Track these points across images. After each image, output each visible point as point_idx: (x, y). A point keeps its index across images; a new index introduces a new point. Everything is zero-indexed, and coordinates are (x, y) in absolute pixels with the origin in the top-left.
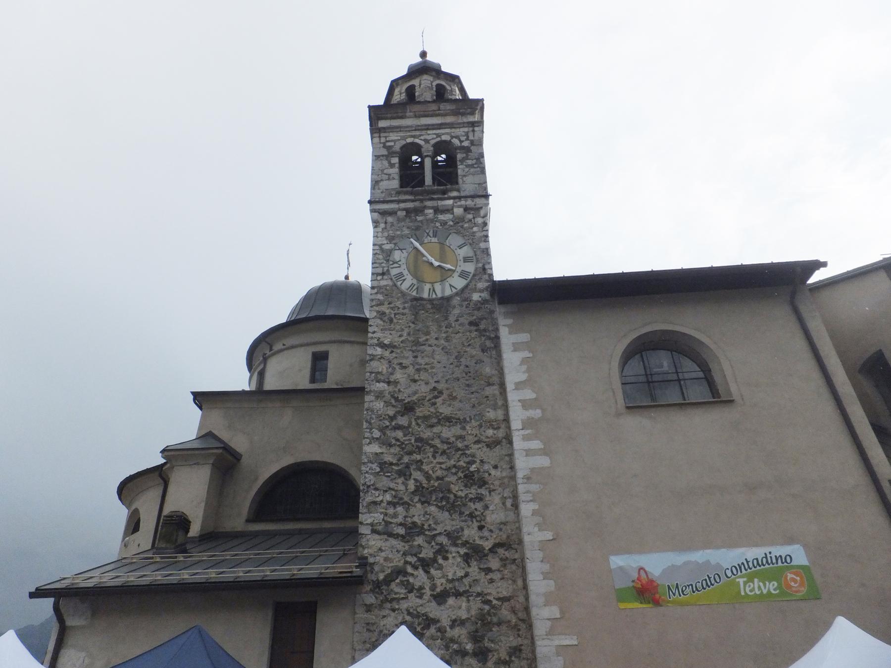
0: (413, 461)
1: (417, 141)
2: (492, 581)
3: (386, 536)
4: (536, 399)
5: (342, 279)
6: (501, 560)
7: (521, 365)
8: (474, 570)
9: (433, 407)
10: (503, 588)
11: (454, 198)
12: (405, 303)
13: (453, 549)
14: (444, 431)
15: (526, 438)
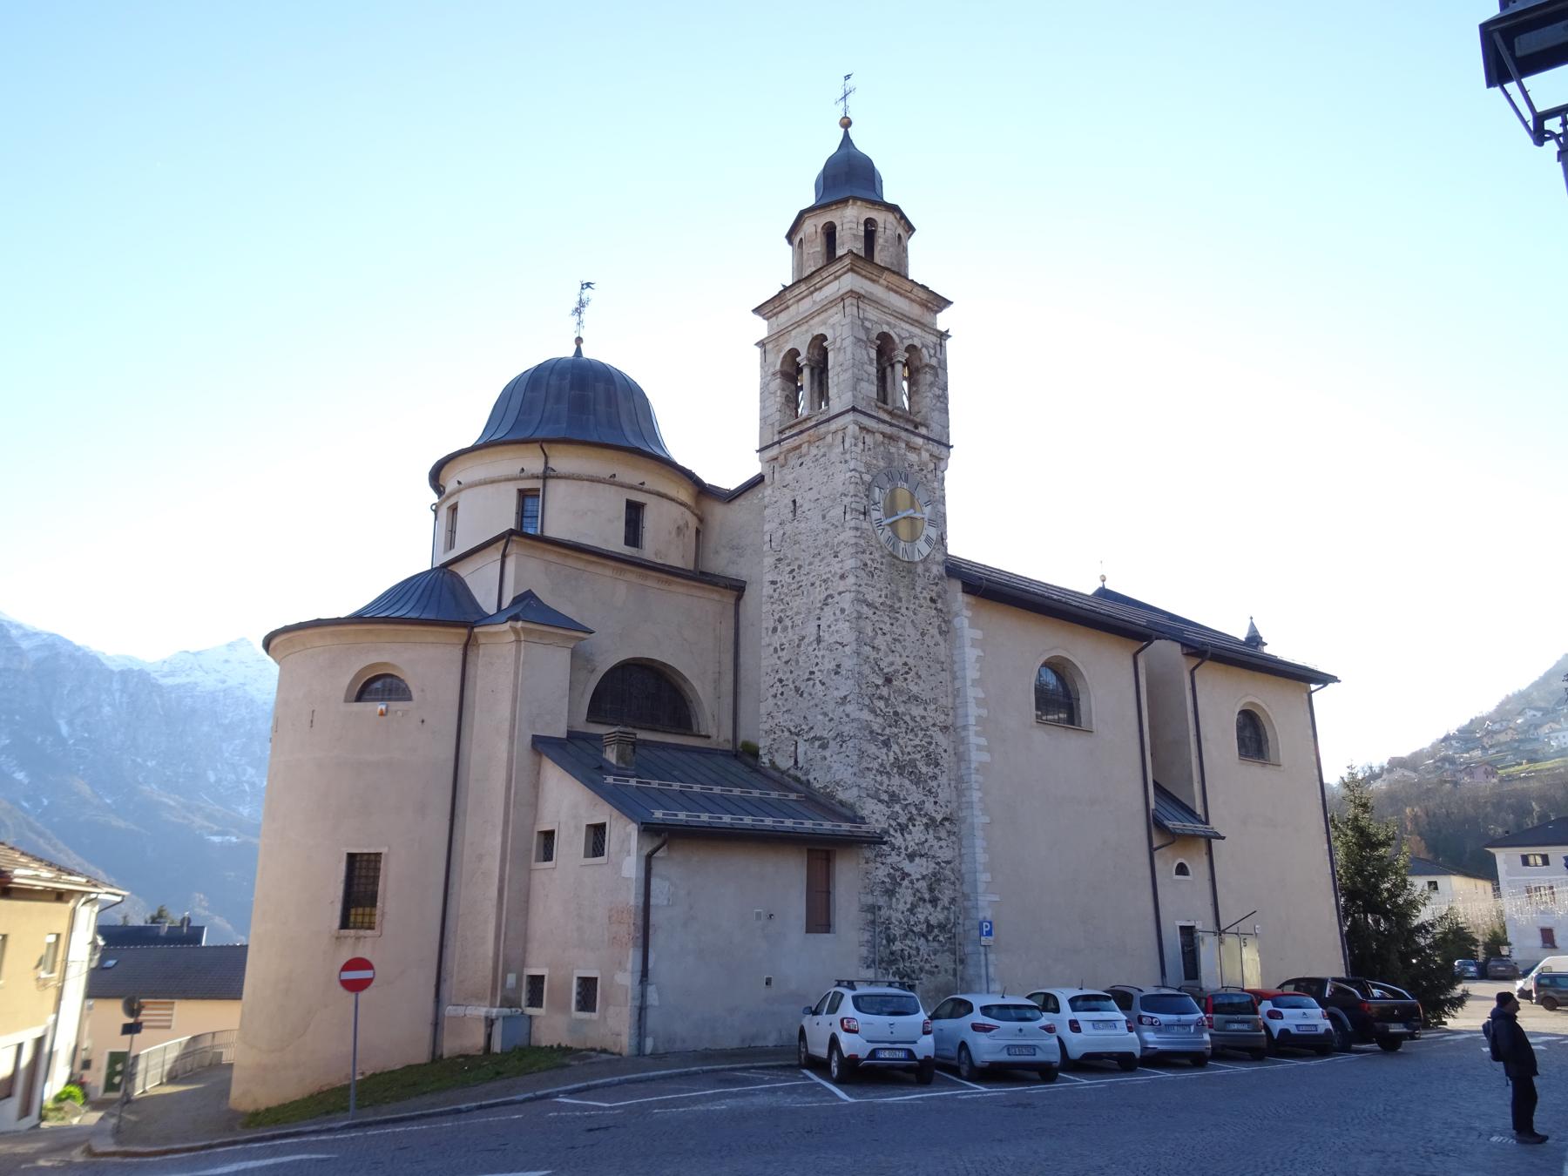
2: (941, 847)
3: (876, 801)
4: (984, 699)
5: (568, 352)
6: (948, 832)
8: (931, 836)
10: (945, 854)
11: (923, 437)
12: (883, 557)
13: (918, 818)
15: (978, 734)
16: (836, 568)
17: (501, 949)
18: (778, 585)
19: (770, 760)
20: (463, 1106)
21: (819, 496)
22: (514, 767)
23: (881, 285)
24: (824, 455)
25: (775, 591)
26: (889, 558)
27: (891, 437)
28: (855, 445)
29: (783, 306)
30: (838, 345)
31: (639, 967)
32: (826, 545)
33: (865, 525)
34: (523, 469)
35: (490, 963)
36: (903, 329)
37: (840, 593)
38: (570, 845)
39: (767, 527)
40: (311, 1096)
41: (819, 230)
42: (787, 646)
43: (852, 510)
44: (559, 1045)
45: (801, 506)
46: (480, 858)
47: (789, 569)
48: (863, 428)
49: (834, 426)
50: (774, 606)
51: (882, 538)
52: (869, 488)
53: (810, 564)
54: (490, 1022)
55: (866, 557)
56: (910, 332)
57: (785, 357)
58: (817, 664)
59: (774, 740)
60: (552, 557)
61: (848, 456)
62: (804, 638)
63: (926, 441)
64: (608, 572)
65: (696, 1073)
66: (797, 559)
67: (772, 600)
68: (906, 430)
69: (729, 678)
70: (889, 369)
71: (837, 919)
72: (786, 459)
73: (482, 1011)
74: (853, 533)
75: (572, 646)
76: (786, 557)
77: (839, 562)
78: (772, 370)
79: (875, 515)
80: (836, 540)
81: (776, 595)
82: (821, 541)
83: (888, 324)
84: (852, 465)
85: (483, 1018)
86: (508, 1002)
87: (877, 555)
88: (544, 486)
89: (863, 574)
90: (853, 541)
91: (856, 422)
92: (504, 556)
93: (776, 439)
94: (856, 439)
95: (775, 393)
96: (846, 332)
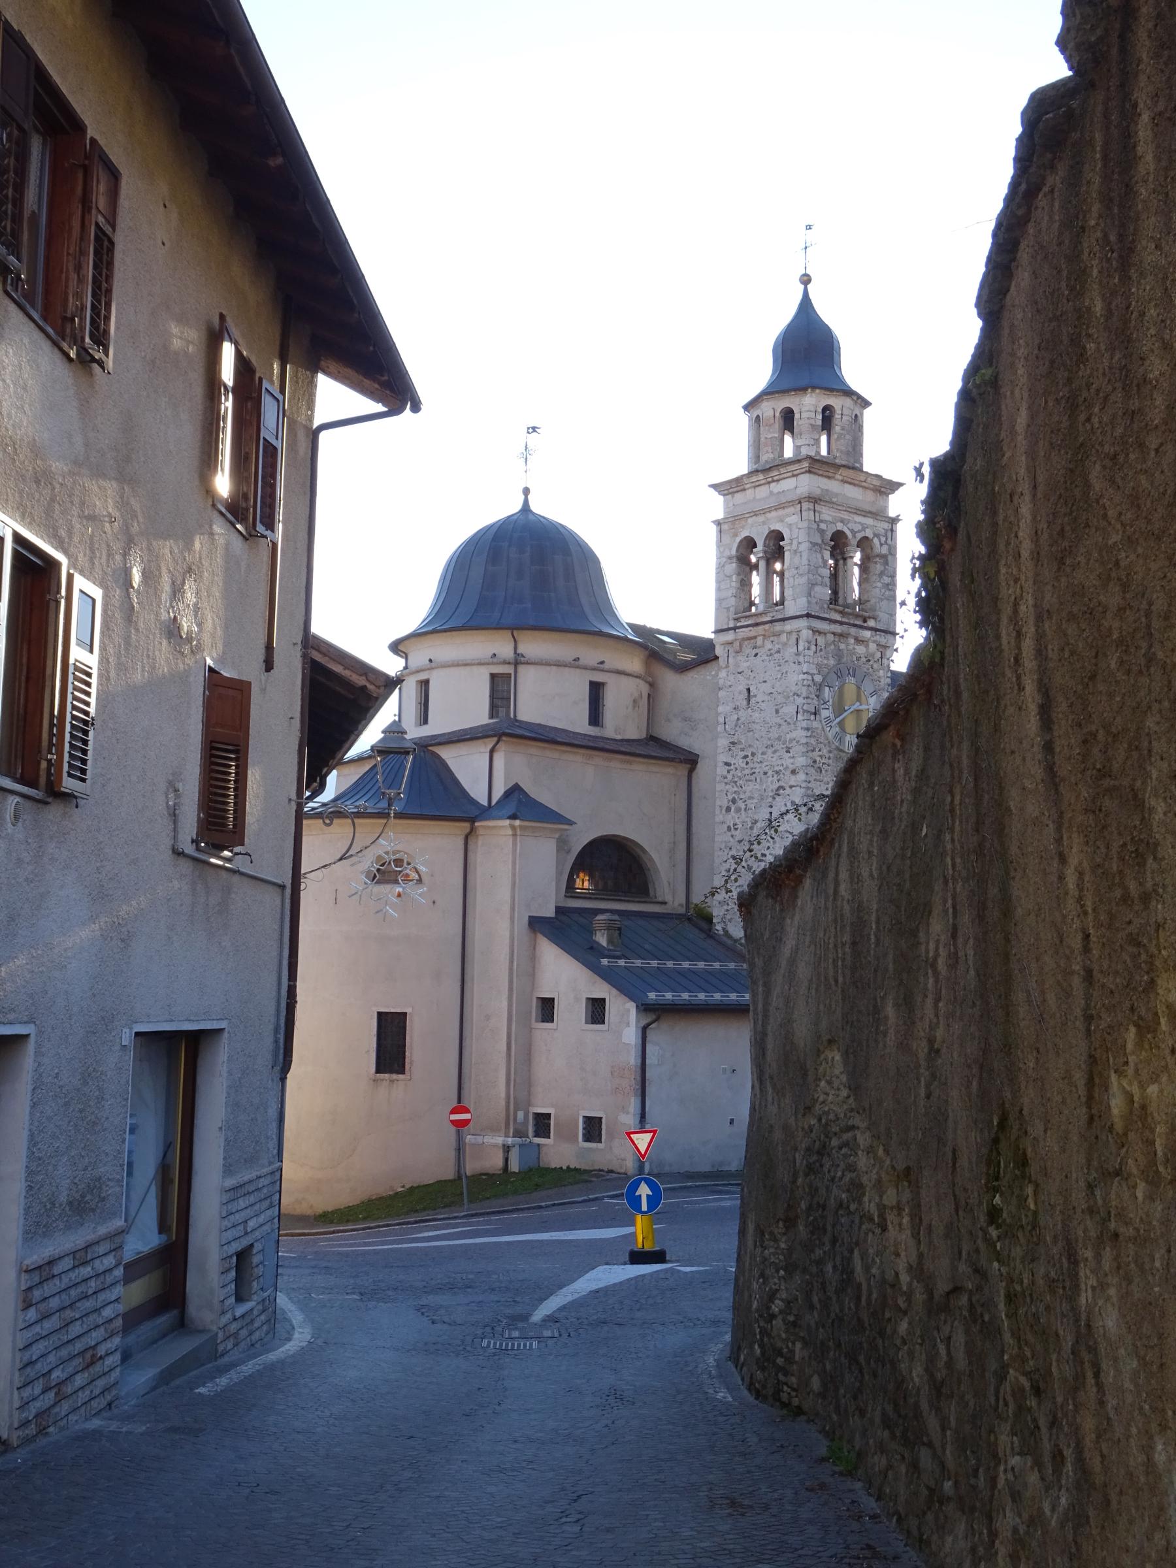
11: (871, 629)
16: (788, 762)
17: (512, 1092)
18: (732, 767)
19: (724, 929)
20: (543, 1204)
21: (772, 691)
22: (516, 944)
23: (838, 480)
24: (778, 652)
25: (728, 772)
26: (835, 752)
27: (841, 635)
28: (809, 649)
29: (739, 488)
30: (794, 547)
31: (639, 1111)
32: (779, 739)
33: (815, 724)
34: (495, 655)
35: (503, 1103)
36: (855, 523)
37: (791, 787)
38: (571, 1012)
39: (720, 709)
40: (381, 1199)
41: (777, 414)
42: (740, 826)
43: (804, 711)
44: (568, 1167)
45: (755, 696)
46: (488, 1018)
47: (743, 754)
48: (816, 632)
49: (789, 626)
50: (727, 787)
51: (830, 735)
52: (820, 688)
53: (763, 753)
54: (507, 1149)
55: (815, 755)
56: (862, 524)
57: (741, 541)
58: (768, 848)
59: (727, 910)
60: (533, 751)
61: (801, 659)
62: (756, 822)
63: (874, 633)
64: (579, 758)
65: (691, 1187)
66: (750, 746)
67: (726, 780)
68: (855, 626)
69: (682, 846)
70: (841, 562)
71: (200, 407)
72: (741, 646)
73: (500, 1140)
74: (804, 733)
75: (557, 836)
76: (740, 742)
77: (790, 757)
78: (727, 553)
79: (825, 713)
80: (788, 736)
81: (730, 777)
82: (774, 734)
83: (842, 521)
84: (805, 668)
85: (500, 1145)
86: (518, 1134)
87: (825, 751)
88: (516, 672)
89: (812, 771)
90: (804, 740)
91: (810, 628)
92: (492, 752)
93: (731, 625)
94: (809, 642)
95: (730, 577)
96: (803, 537)
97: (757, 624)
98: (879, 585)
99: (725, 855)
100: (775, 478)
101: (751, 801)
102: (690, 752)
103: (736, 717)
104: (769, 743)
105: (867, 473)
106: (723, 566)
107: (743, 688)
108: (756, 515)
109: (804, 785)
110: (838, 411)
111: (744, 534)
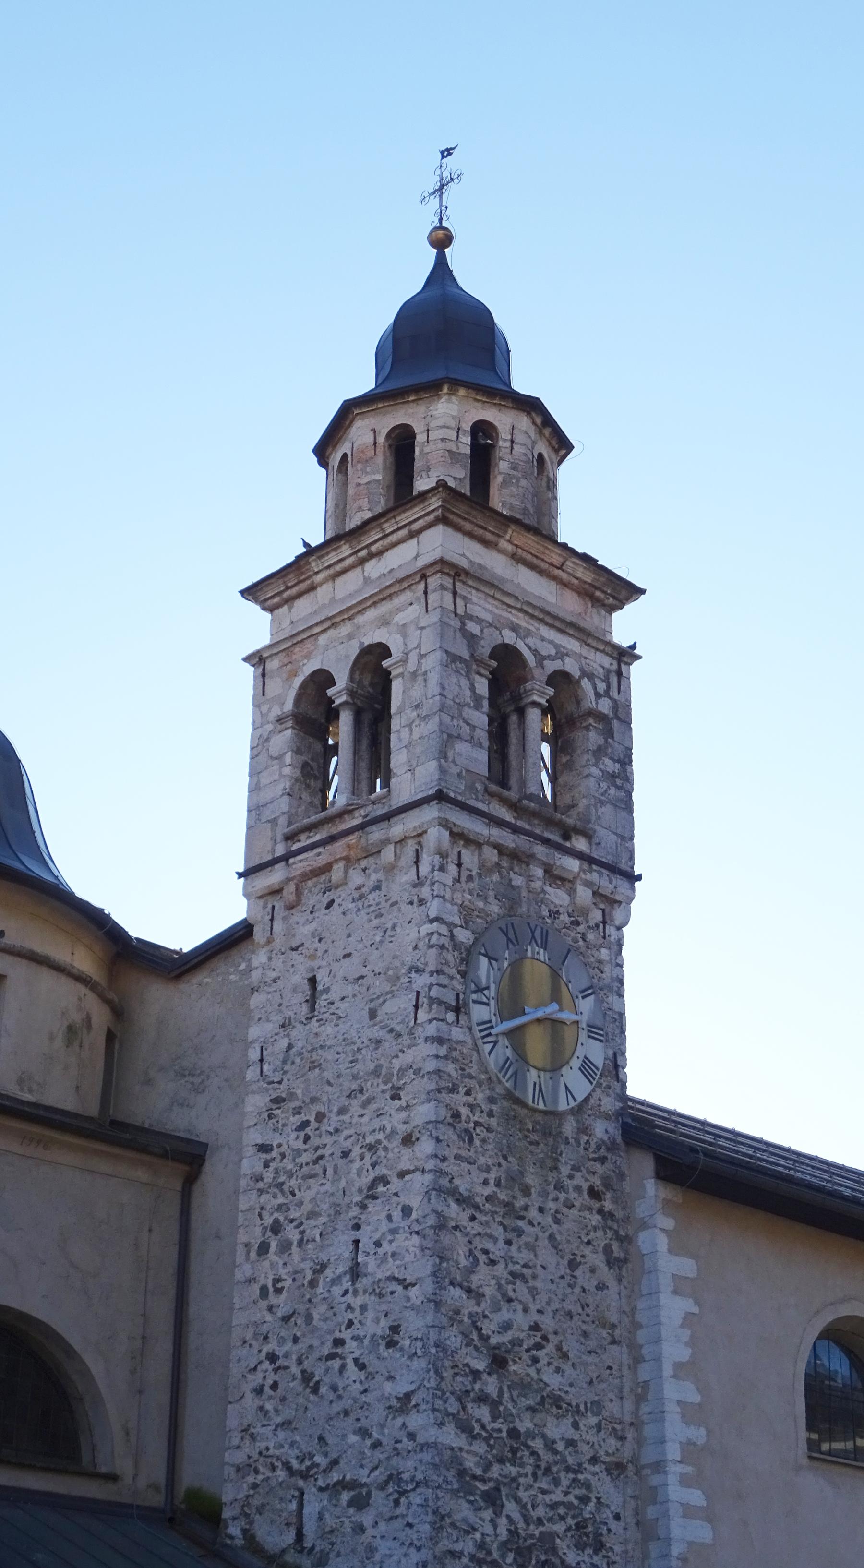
0: (505, 1477)
1: (521, 646)
7: (682, 1326)
9: (533, 1368)
14: (549, 1425)
15: (685, 1481)
16: (395, 1120)
18: (275, 1153)
19: (245, 1531)
21: (364, 971)
23: (502, 551)
24: (377, 888)
25: (266, 1165)
28: (442, 869)
29: (303, 586)
30: (411, 666)
32: (376, 1072)
33: (457, 1033)
37: (402, 1175)
39: (255, 1032)
41: (381, 439)
45: (327, 990)
47: (296, 1120)
48: (457, 835)
49: (398, 828)
50: (264, 1198)
51: (492, 1062)
52: (467, 957)
53: (342, 1111)
56: (556, 646)
57: (304, 686)
59: (255, 1486)
61: (425, 892)
62: (323, 1267)
63: (586, 866)
66: (314, 1100)
67: (260, 1185)
68: (546, 842)
69: (163, 1348)
72: (298, 892)
74: (432, 1049)
77: (401, 1109)
78: (276, 711)
79: (480, 1013)
80: (397, 1064)
81: (268, 1176)
82: (366, 1065)
83: (514, 628)
87: (480, 1096)
89: (450, 1135)
90: (431, 1065)
91: (444, 823)
93: (280, 850)
94: (443, 855)
95: (280, 757)
96: (429, 641)
97: (332, 839)
98: (595, 771)
99: (249, 1356)
100: (374, 548)
101: (312, 1222)
102: (189, 1141)
103: (284, 1043)
104: (354, 1086)
105: (564, 546)
106: (267, 740)
107: (299, 978)
108: (334, 625)
109: (431, 1164)
110: (504, 434)
111: (309, 668)
